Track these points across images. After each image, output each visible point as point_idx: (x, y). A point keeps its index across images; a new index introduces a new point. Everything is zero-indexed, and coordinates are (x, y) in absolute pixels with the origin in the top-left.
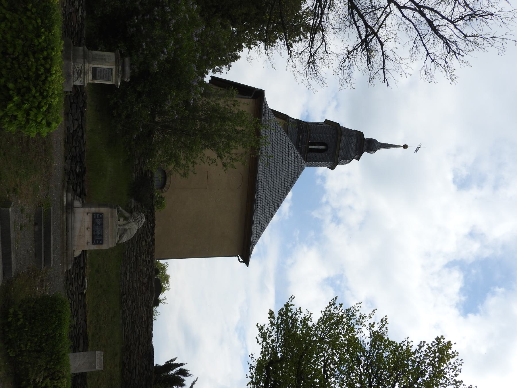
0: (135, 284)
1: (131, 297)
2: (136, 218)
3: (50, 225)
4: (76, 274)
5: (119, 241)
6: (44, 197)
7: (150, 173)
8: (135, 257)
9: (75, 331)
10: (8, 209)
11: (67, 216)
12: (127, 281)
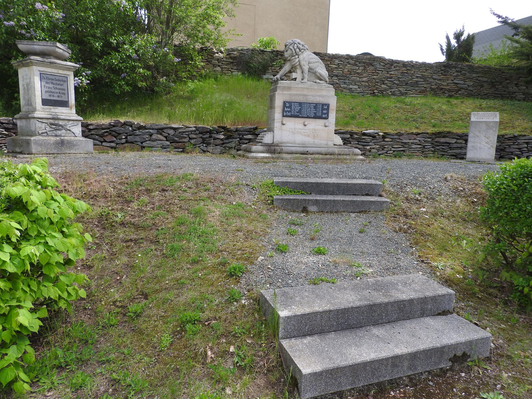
0: (364, 79)
1: (377, 85)
2: (294, 52)
3: (306, 183)
4: (358, 144)
5: (326, 82)
6: (255, 194)
7: (232, 53)
8: (332, 77)
9: (428, 147)
10: (281, 321)
11: (286, 153)
12: (359, 88)
